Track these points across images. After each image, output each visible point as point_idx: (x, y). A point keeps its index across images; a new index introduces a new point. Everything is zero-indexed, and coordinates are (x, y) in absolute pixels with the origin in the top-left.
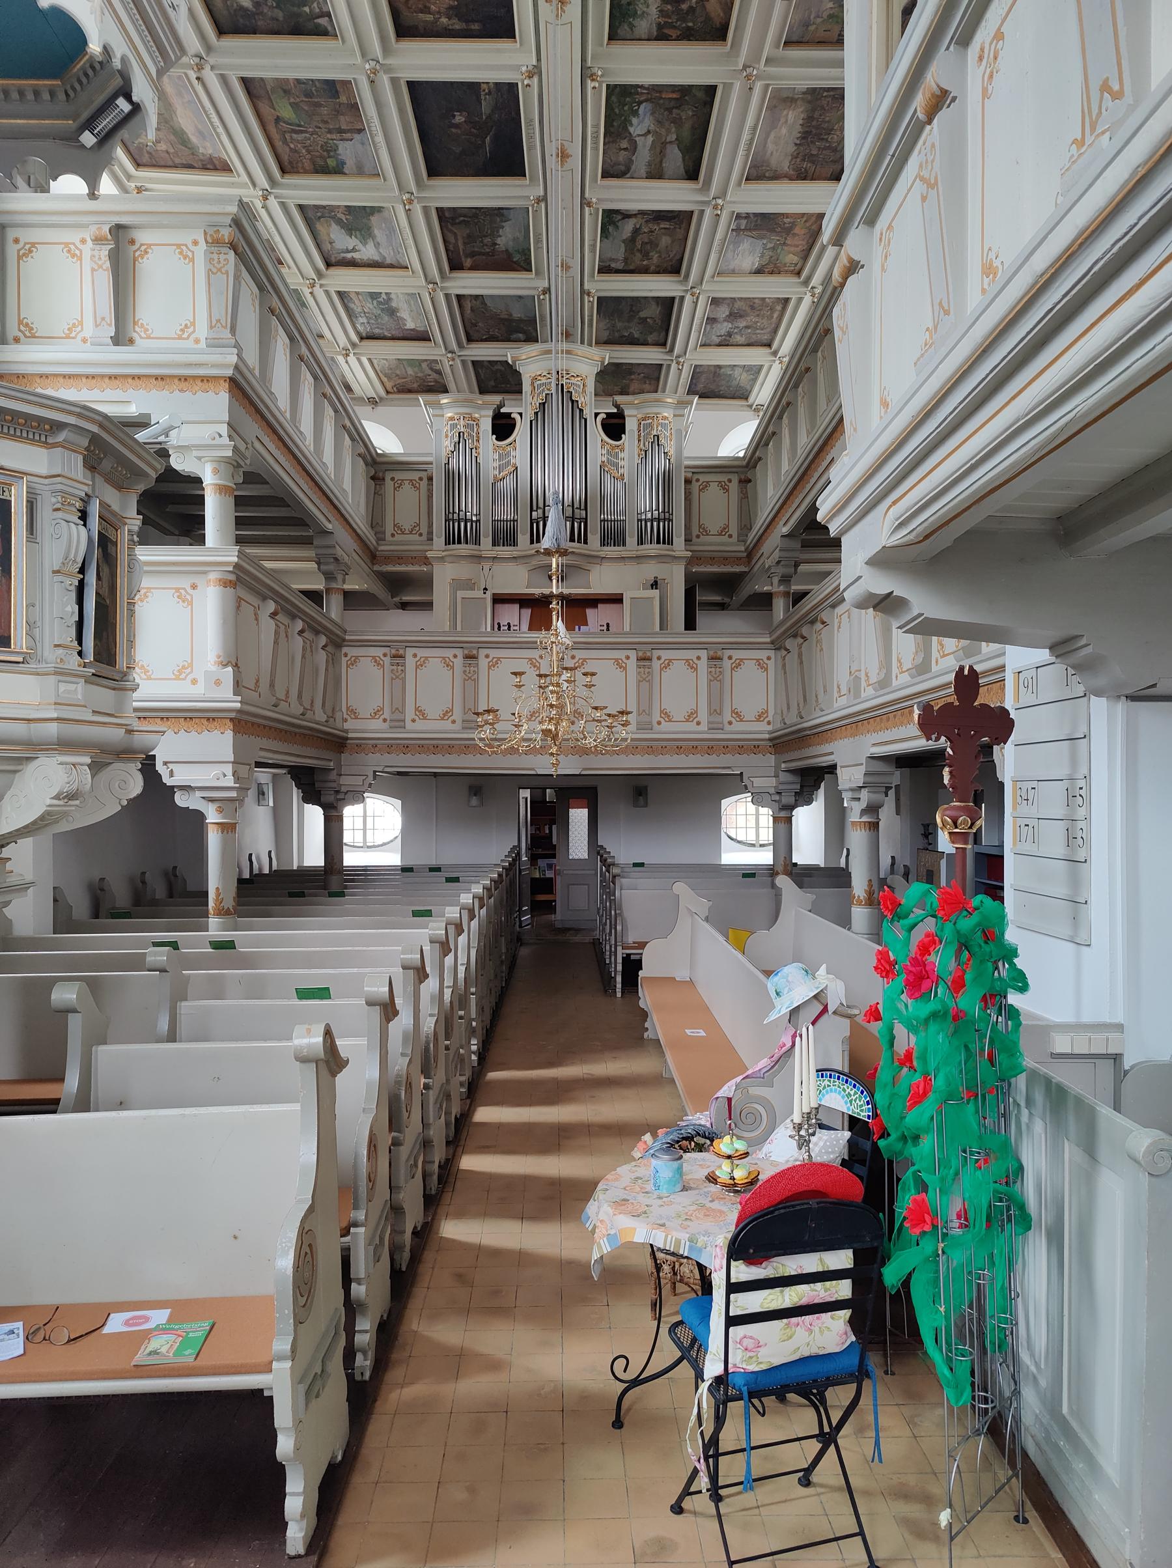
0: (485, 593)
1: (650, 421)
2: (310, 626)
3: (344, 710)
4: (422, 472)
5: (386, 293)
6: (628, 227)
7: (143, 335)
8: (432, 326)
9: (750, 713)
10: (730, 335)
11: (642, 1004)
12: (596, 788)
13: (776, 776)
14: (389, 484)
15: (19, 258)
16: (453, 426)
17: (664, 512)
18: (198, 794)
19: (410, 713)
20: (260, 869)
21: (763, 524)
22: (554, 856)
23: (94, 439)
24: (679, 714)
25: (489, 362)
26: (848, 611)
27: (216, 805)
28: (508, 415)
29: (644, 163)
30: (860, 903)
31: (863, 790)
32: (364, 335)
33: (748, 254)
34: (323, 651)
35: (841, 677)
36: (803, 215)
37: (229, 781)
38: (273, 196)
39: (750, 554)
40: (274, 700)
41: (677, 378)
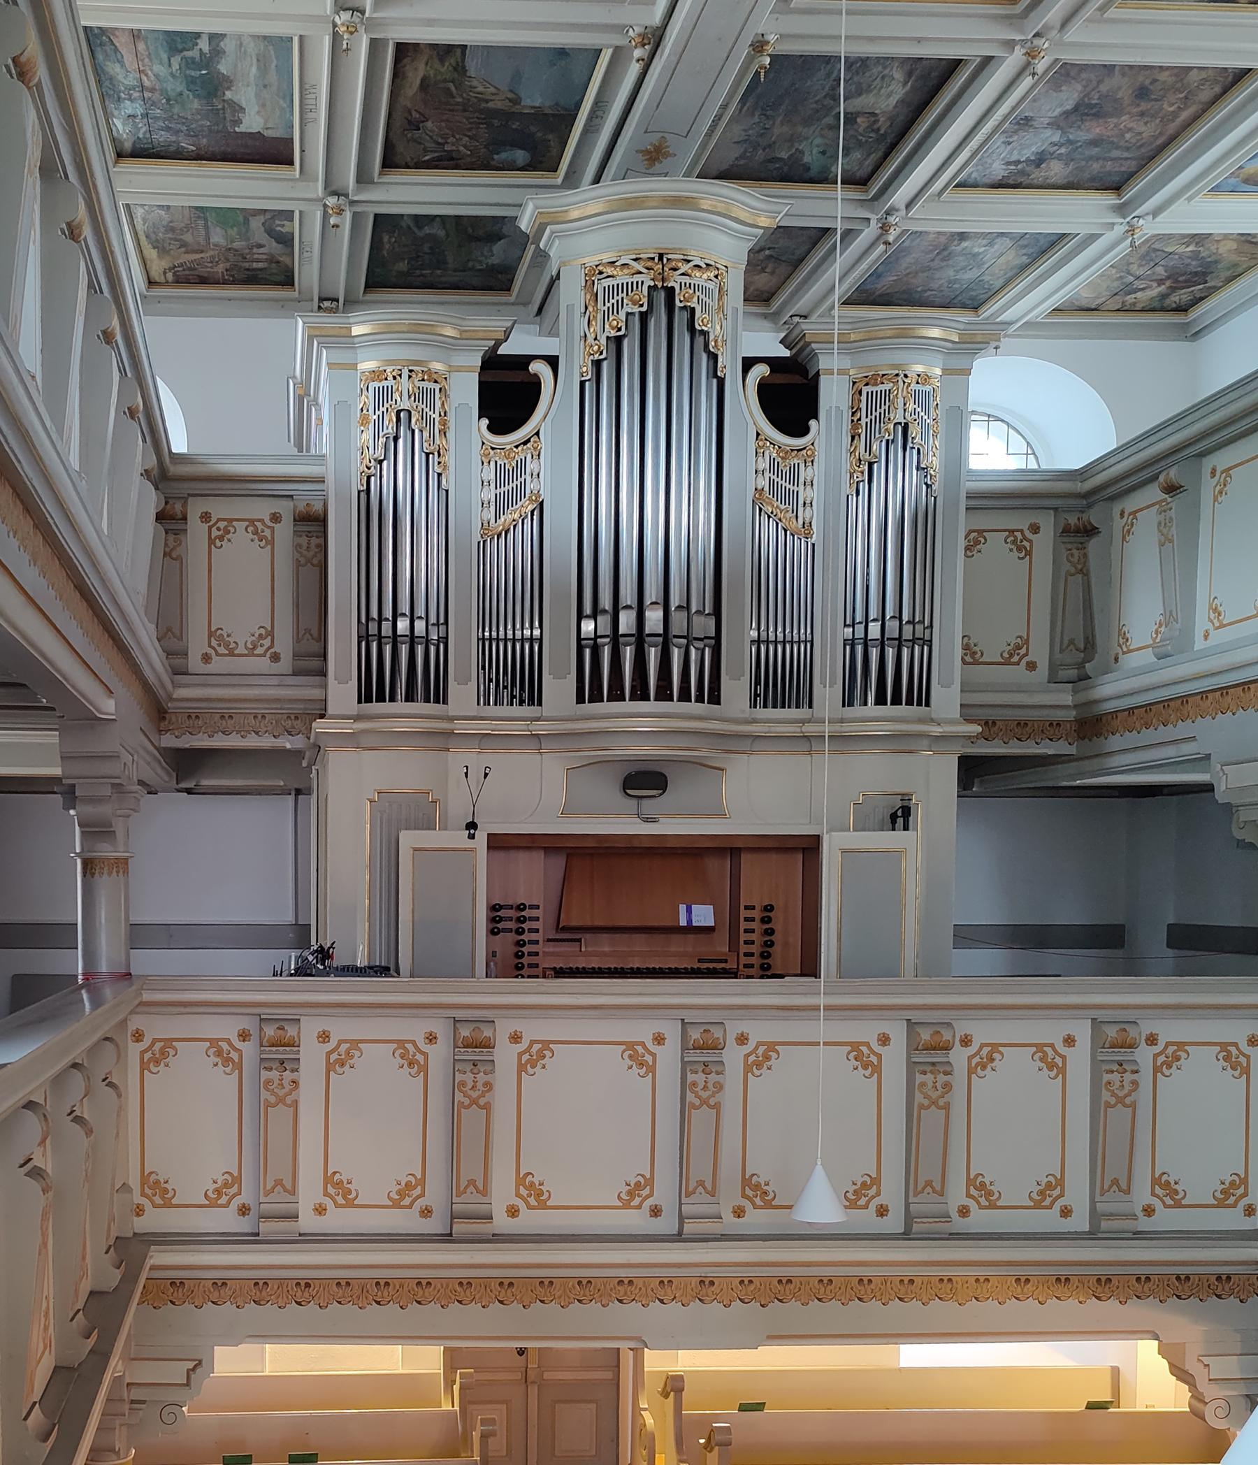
0: (472, 837)
3: (134, 1182)
8: (309, 128)
14: (196, 531)
16: (383, 396)
32: (128, 146)
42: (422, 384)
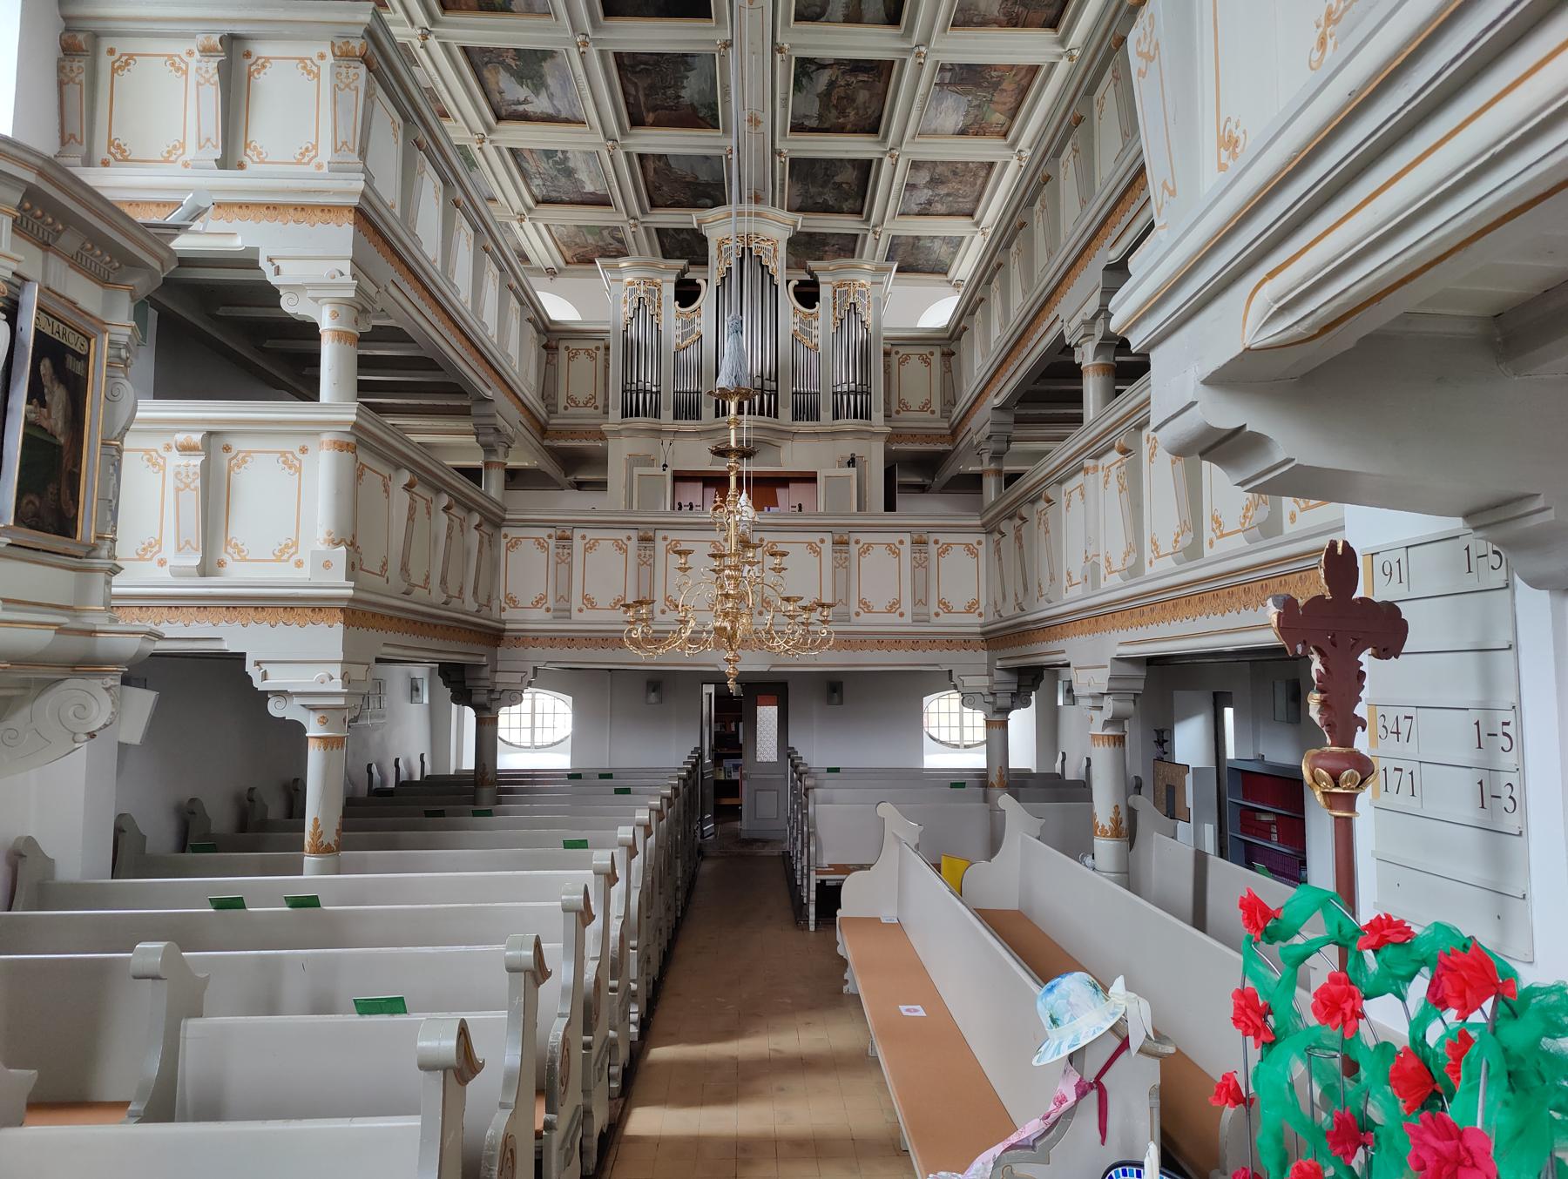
0: (664, 470)
1: (847, 288)
2: (457, 501)
3: (502, 597)
4: (598, 341)
5: (563, 152)
6: (824, 78)
7: (255, 159)
8: (612, 189)
9: (959, 604)
10: (930, 203)
11: (840, 950)
12: (787, 683)
13: (990, 675)
14: (563, 354)
15: (114, 71)
17: (861, 384)
18: (297, 701)
19: (576, 601)
20: (411, 775)
21: (970, 397)
22: (740, 756)
23: (31, 193)
24: (880, 604)
25: (675, 230)
26: (1080, 486)
27: (318, 715)
28: (693, 282)
29: (840, 5)
30: (1104, 834)
31: (1106, 697)
32: (540, 198)
33: (951, 113)
34: (476, 532)
35: (1073, 561)
36: (1013, 67)
37: (337, 686)
38: (433, 36)
39: (955, 431)
40: (405, 587)
41: (874, 250)
42: (649, 287)
